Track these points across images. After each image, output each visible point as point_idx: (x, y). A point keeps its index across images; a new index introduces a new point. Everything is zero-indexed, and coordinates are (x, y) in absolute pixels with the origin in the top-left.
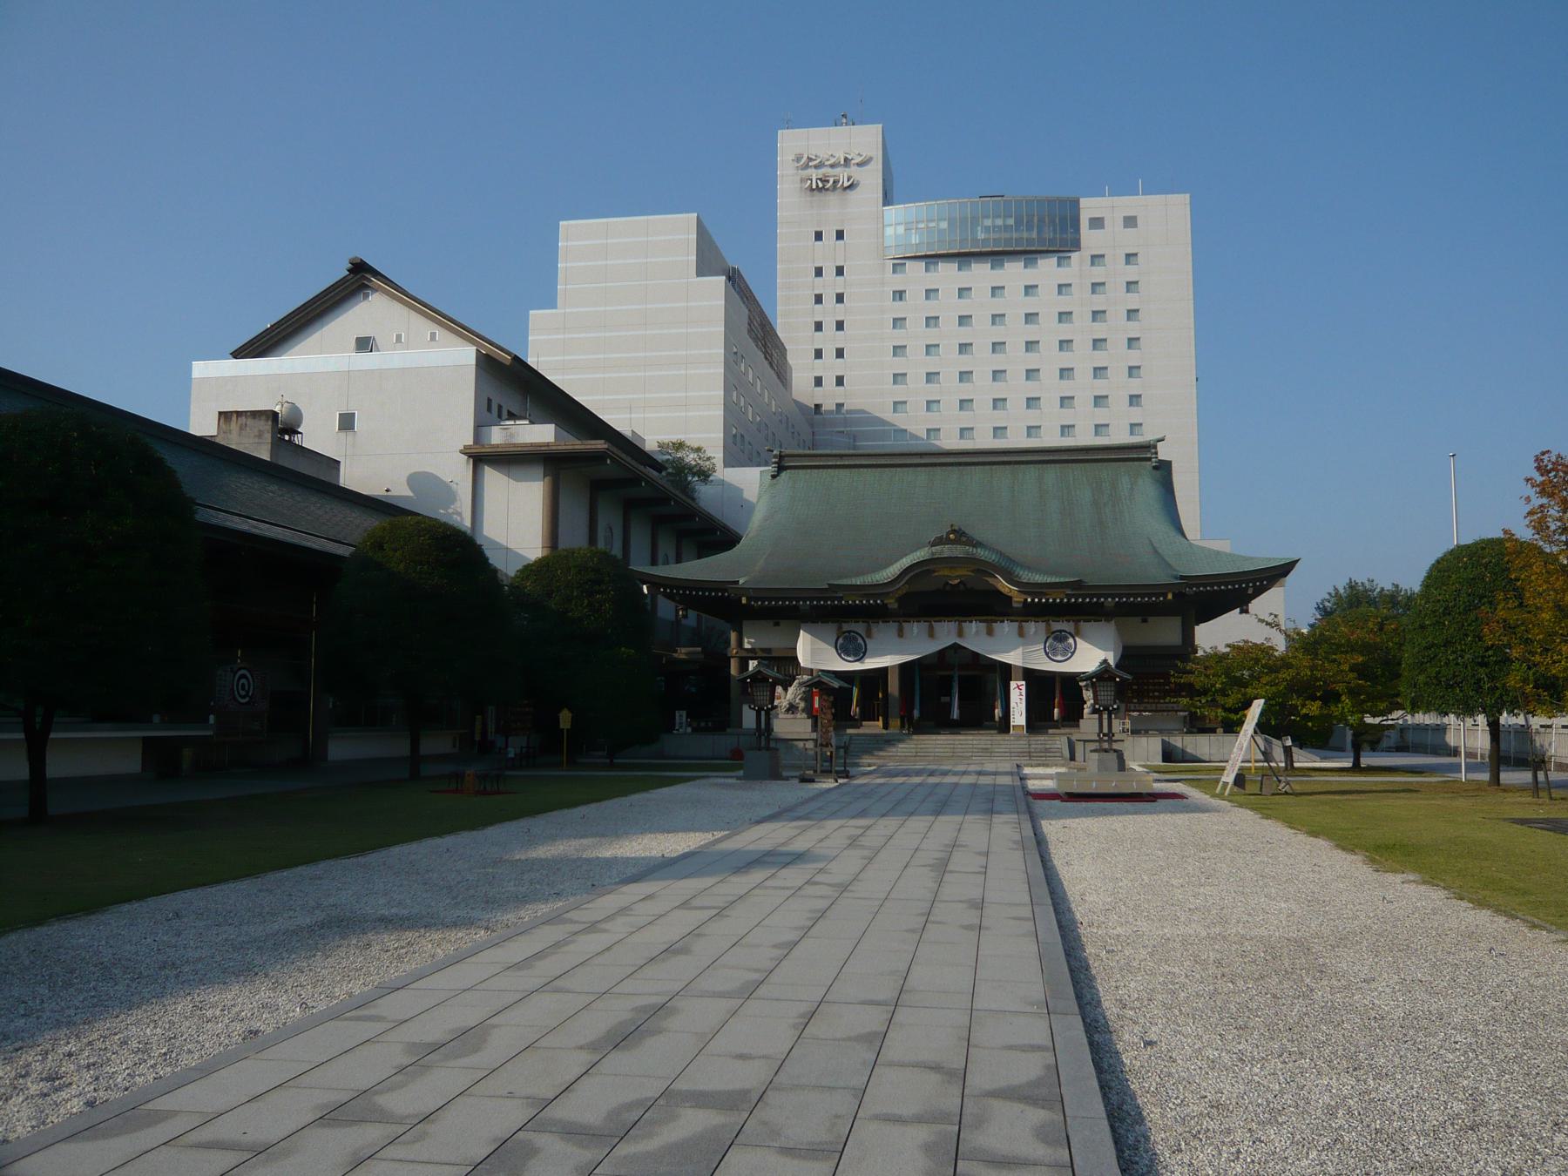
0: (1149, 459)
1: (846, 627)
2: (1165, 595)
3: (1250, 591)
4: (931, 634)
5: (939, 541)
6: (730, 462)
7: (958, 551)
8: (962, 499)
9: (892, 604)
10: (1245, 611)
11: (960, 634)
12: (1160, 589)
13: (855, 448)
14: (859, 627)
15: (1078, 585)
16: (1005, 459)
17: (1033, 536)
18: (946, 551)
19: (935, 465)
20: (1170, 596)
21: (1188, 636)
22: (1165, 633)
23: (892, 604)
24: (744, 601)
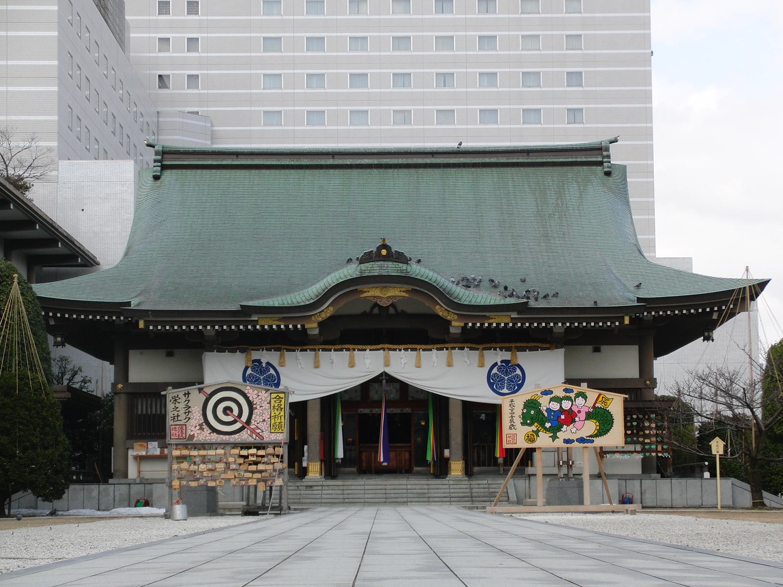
0: (601, 163)
1: (255, 355)
2: (621, 320)
3: (715, 316)
4: (352, 365)
5: (367, 258)
6: (68, 152)
7: (391, 268)
8: (389, 211)
9: (313, 327)
10: (708, 338)
11: (387, 364)
12: (619, 311)
13: (213, 137)
14: (266, 357)
15: (522, 308)
16: (493, 160)
17: (466, 251)
18: (375, 268)
19: (350, 167)
20: (627, 321)
21: (645, 368)
22: (176, 493)
23: (313, 327)
24: (141, 325)
